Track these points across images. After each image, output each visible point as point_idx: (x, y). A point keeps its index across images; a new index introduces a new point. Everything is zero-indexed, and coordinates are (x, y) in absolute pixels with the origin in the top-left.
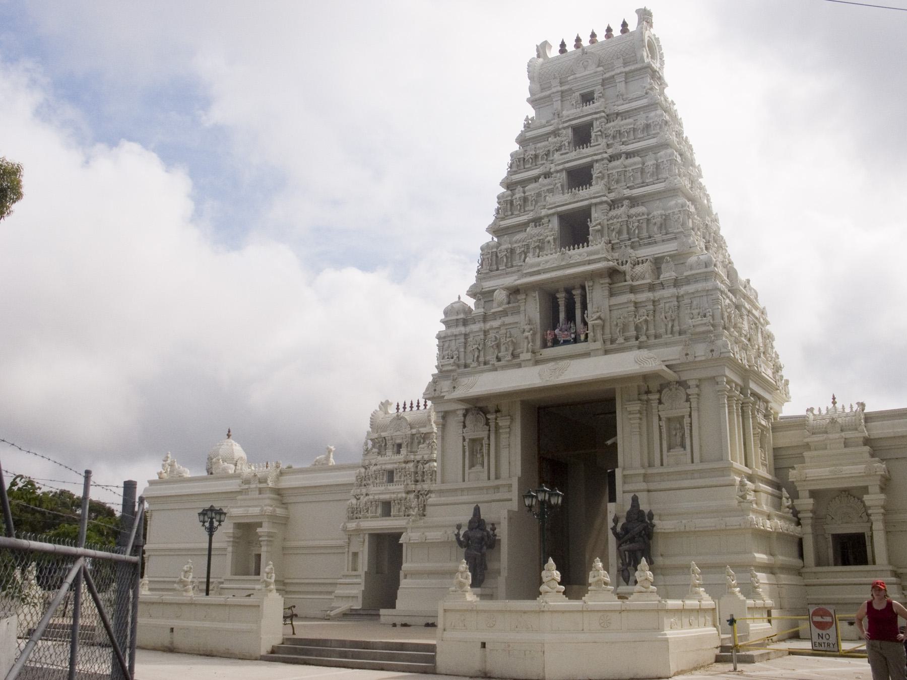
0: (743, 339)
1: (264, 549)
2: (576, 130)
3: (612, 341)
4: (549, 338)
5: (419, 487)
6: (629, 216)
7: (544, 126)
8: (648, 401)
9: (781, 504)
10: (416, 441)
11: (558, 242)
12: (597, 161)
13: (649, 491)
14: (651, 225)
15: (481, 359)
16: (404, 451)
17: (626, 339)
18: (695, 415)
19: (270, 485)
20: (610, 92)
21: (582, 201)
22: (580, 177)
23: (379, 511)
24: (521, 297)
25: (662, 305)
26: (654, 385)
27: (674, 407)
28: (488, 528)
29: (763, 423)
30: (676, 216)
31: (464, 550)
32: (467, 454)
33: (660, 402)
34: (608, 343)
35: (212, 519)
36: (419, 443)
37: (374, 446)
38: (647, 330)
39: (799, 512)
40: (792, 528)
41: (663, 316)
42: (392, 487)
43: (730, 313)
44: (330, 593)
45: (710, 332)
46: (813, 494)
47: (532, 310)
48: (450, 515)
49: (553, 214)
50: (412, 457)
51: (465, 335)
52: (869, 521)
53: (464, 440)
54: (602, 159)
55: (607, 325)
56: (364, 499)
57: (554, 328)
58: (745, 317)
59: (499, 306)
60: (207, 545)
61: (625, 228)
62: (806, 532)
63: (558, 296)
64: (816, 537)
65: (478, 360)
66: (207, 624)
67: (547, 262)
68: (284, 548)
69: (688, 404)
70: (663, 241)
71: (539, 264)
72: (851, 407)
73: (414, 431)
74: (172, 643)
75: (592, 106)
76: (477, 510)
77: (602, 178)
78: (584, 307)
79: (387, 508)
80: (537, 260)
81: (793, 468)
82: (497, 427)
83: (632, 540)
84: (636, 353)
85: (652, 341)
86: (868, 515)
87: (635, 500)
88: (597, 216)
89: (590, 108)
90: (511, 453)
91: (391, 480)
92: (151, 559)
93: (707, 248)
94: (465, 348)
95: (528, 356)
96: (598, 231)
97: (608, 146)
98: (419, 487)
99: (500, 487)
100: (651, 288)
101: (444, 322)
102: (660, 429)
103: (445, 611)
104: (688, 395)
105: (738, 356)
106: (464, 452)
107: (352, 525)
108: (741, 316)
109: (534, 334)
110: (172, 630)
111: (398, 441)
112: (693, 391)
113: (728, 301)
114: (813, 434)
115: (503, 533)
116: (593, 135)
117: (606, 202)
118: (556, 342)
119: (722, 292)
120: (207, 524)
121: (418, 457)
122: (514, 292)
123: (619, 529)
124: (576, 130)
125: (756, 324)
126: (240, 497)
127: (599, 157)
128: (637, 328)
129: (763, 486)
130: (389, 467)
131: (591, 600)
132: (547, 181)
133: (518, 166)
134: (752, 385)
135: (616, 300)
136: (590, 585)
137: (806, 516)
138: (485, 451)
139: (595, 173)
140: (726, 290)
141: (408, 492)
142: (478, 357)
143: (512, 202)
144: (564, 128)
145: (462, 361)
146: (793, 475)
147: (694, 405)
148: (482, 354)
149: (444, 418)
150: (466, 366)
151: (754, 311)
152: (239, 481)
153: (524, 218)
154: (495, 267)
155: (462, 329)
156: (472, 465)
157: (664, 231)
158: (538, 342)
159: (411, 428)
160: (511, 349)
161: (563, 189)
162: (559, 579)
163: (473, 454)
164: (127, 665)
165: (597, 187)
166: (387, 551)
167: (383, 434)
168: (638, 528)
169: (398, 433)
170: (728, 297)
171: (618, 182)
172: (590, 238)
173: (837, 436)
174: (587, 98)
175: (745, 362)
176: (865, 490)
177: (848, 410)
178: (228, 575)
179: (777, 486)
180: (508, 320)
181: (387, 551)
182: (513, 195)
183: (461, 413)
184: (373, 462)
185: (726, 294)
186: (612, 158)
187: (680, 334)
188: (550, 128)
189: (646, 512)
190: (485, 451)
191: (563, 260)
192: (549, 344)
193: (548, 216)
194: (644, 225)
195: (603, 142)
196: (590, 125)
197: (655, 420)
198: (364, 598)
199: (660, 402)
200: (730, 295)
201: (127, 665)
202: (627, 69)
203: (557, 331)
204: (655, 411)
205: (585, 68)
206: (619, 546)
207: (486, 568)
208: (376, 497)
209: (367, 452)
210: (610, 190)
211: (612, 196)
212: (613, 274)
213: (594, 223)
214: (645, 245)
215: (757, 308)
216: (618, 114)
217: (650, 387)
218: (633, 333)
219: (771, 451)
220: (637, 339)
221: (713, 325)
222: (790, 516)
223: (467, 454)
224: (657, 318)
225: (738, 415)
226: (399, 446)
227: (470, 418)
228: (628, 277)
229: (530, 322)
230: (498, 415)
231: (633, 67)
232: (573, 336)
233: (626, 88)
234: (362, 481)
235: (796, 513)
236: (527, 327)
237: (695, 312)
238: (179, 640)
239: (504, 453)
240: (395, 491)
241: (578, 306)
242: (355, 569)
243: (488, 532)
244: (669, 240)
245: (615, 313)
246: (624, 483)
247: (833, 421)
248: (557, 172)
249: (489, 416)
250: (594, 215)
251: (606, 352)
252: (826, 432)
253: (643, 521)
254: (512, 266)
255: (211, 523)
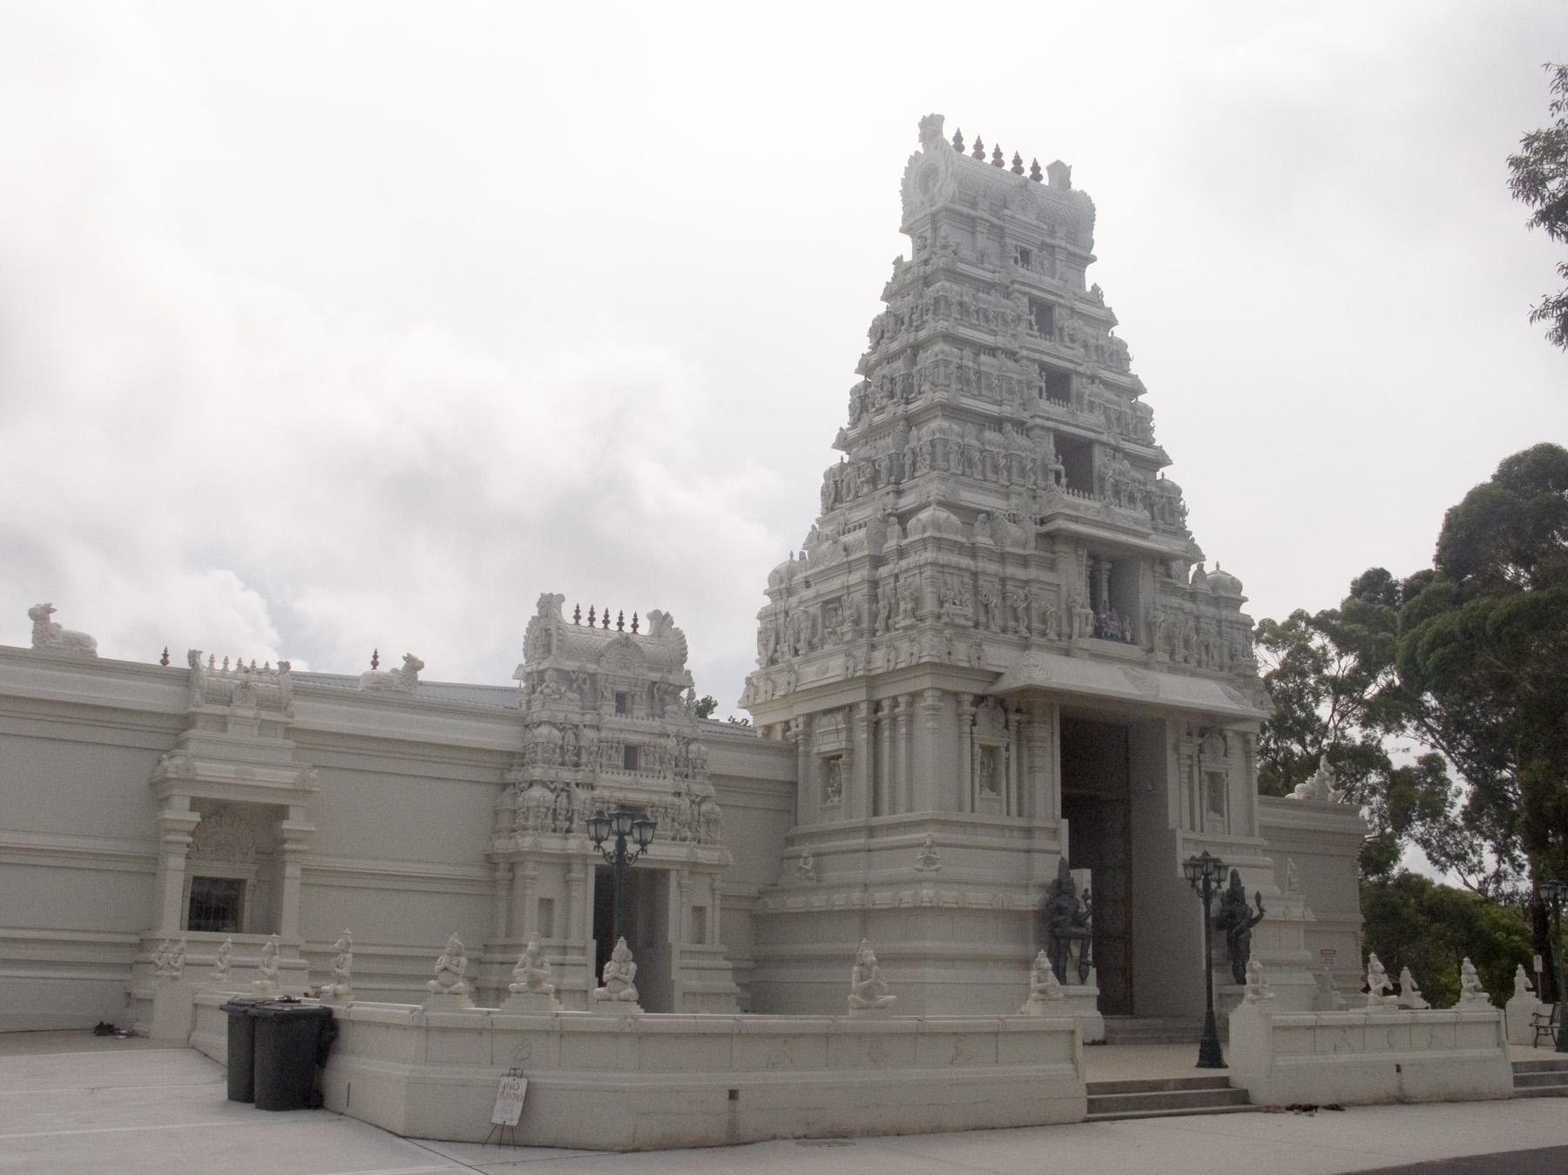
21: (1078, 426)
66: (1344, 1058)
70: (1164, 531)
72: (226, 662)
74: (1401, 1089)
110: (1398, 1069)
111: (623, 688)
120: (1200, 884)
130: (634, 739)
173: (250, 713)
177: (219, 666)
238: (1414, 1083)
247: (245, 686)
252: (229, 703)
255: (1207, 883)
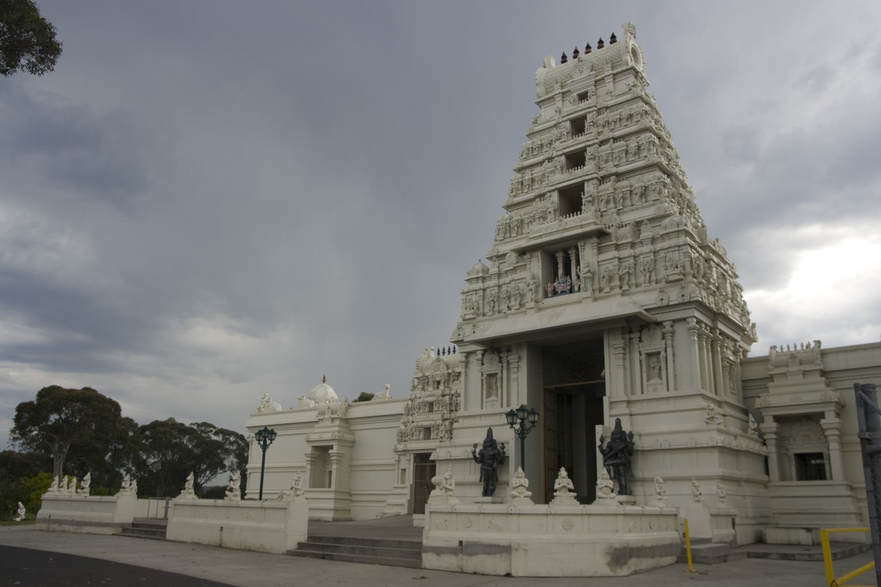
0: (711, 286)
1: (334, 466)
2: (573, 122)
3: (600, 290)
4: (550, 289)
5: (453, 416)
6: (615, 189)
7: (549, 121)
8: (631, 339)
9: (748, 427)
10: (451, 378)
11: (558, 213)
12: (590, 146)
13: (631, 415)
14: (634, 196)
15: (496, 309)
16: (441, 387)
17: (612, 289)
18: (669, 350)
19: (340, 416)
20: (602, 91)
22: (576, 159)
23: (422, 436)
24: (527, 256)
25: (641, 259)
27: (653, 343)
28: (499, 447)
29: (731, 358)
30: (654, 187)
31: (480, 465)
32: (485, 386)
34: (597, 292)
35: (265, 438)
36: (454, 380)
37: (419, 383)
38: (629, 280)
39: (764, 434)
40: (756, 447)
41: (642, 269)
42: (432, 416)
43: (698, 265)
44: (384, 501)
45: (681, 280)
46: (778, 419)
47: (536, 266)
48: (471, 437)
49: (553, 190)
50: (447, 392)
51: (484, 290)
52: (826, 442)
53: (482, 375)
54: (594, 144)
55: (596, 277)
56: (410, 426)
57: (555, 281)
58: (714, 269)
59: (510, 265)
61: (612, 197)
62: (771, 450)
64: (780, 455)
65: (493, 311)
67: (547, 228)
68: (351, 466)
69: (663, 342)
70: (643, 207)
71: (541, 231)
73: (450, 371)
74: (221, 540)
75: (586, 102)
76: (490, 433)
77: (594, 159)
78: (578, 263)
79: (428, 431)
80: (540, 227)
81: (759, 397)
82: (508, 363)
83: (615, 456)
84: (619, 299)
85: (634, 289)
86: (826, 437)
87: (618, 423)
88: (589, 188)
89: (585, 104)
90: (519, 386)
91: (431, 410)
92: (252, 475)
93: (680, 213)
94: (483, 300)
95: (532, 305)
96: (589, 202)
97: (599, 133)
98: (453, 416)
99: (495, 406)
100: (633, 245)
102: (641, 363)
103: (431, 512)
105: (706, 301)
106: (482, 385)
107: (401, 447)
108: (710, 268)
109: (538, 287)
111: (438, 379)
112: (668, 328)
113: (697, 255)
114: (776, 367)
115: (511, 451)
116: (586, 125)
117: (596, 178)
118: (555, 293)
119: (692, 247)
120: (262, 443)
121: (453, 392)
122: (522, 252)
123: (605, 447)
124: (573, 122)
125: (724, 275)
126: (317, 425)
127: (591, 143)
128: (621, 279)
129: (728, 410)
130: (430, 399)
131: (555, 506)
132: (550, 164)
133: (528, 154)
134: (721, 326)
135: (603, 257)
136: (556, 491)
137: (771, 437)
138: (499, 384)
139: (588, 155)
140: (696, 246)
141: (444, 420)
142: (494, 307)
143: (522, 182)
144: (564, 121)
145: (481, 311)
146: (758, 403)
147: (669, 342)
148: (496, 304)
149: (467, 357)
150: (484, 315)
151: (722, 265)
152: (316, 413)
153: (531, 195)
154: (508, 235)
155: (480, 285)
156: (489, 396)
157: (644, 200)
158: (541, 295)
159: (448, 368)
160: (519, 299)
161: (562, 170)
162: (527, 485)
163: (489, 387)
165: (589, 167)
166: (425, 465)
167: (427, 374)
168: (619, 446)
169: (438, 372)
170: (698, 252)
171: (607, 161)
172: (583, 207)
174: (583, 97)
175: (713, 306)
176: (822, 415)
178: (307, 488)
179: (746, 412)
180: (517, 276)
181: (425, 465)
182: (523, 177)
183: (479, 354)
184: (418, 396)
185: (696, 249)
186: (602, 143)
187: (657, 282)
188: (553, 123)
189: (628, 432)
190: (499, 384)
191: (560, 225)
192: (550, 295)
193: (550, 191)
194: (628, 195)
195: (594, 130)
196: (584, 117)
197: (637, 355)
198: (409, 506)
199: (641, 341)
200: (699, 249)
202: (615, 72)
203: (555, 284)
204: (636, 347)
205: (581, 72)
206: (605, 461)
207: (497, 480)
208: (420, 424)
209: (414, 388)
210: (600, 169)
211: (602, 173)
212: (601, 235)
213: (586, 195)
215: (725, 263)
216: (607, 108)
217: (633, 326)
218: (617, 282)
219: (740, 383)
220: (621, 287)
221: (684, 275)
222: (756, 437)
223: (485, 386)
224: (638, 271)
225: (708, 351)
226: (439, 383)
227: (487, 356)
228: (613, 238)
229: (533, 278)
231: (619, 70)
232: (569, 287)
233: (614, 87)
234: (409, 411)
235: (761, 435)
236: (531, 282)
237: (668, 264)
239: (514, 385)
240: (434, 419)
241: (573, 262)
242: (403, 482)
243: (499, 451)
244: (647, 206)
245: (603, 268)
246: (611, 409)
248: (558, 156)
249: (502, 355)
250: (586, 188)
251: (595, 299)
252: (787, 366)
253: (625, 440)
254: (522, 234)
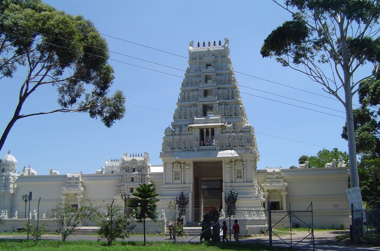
26: (233, 160)
33: (235, 165)
60: (25, 211)
63: (209, 130)
101: (346, 140)
104: (243, 164)
120: (124, 198)
164: (234, 231)
199: (235, 165)
201: (234, 231)
214: (229, 118)
230: (185, 165)
